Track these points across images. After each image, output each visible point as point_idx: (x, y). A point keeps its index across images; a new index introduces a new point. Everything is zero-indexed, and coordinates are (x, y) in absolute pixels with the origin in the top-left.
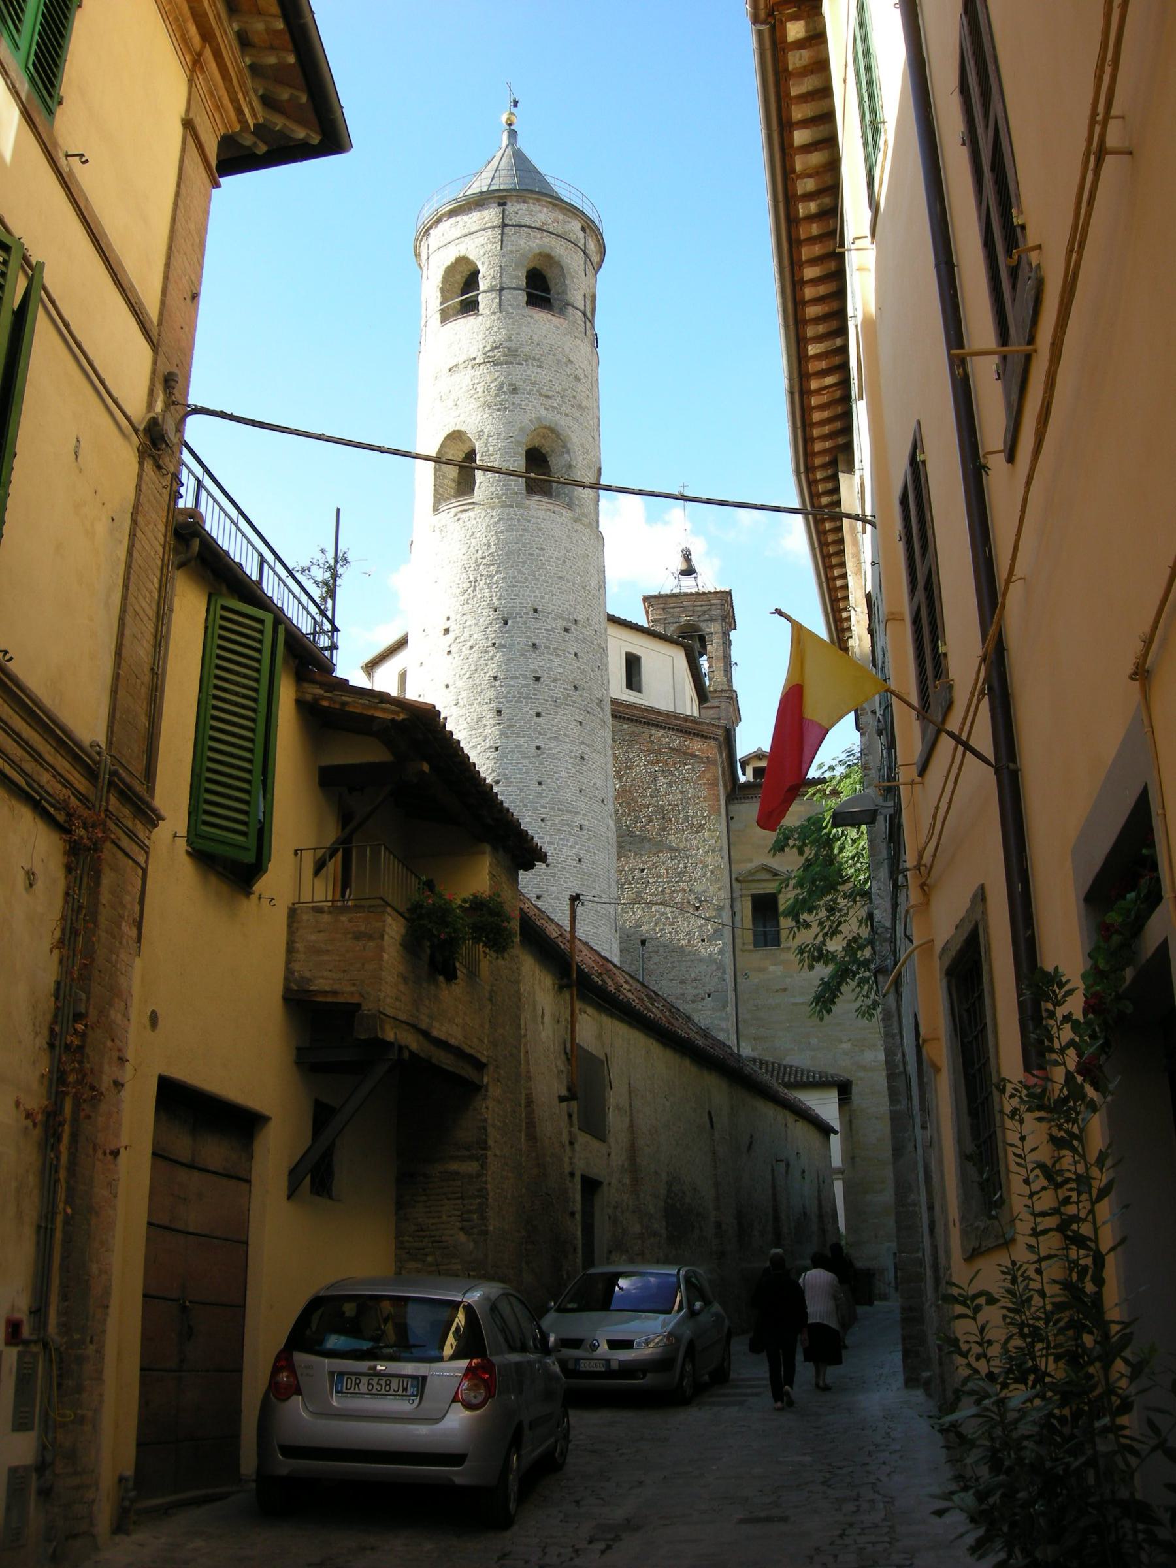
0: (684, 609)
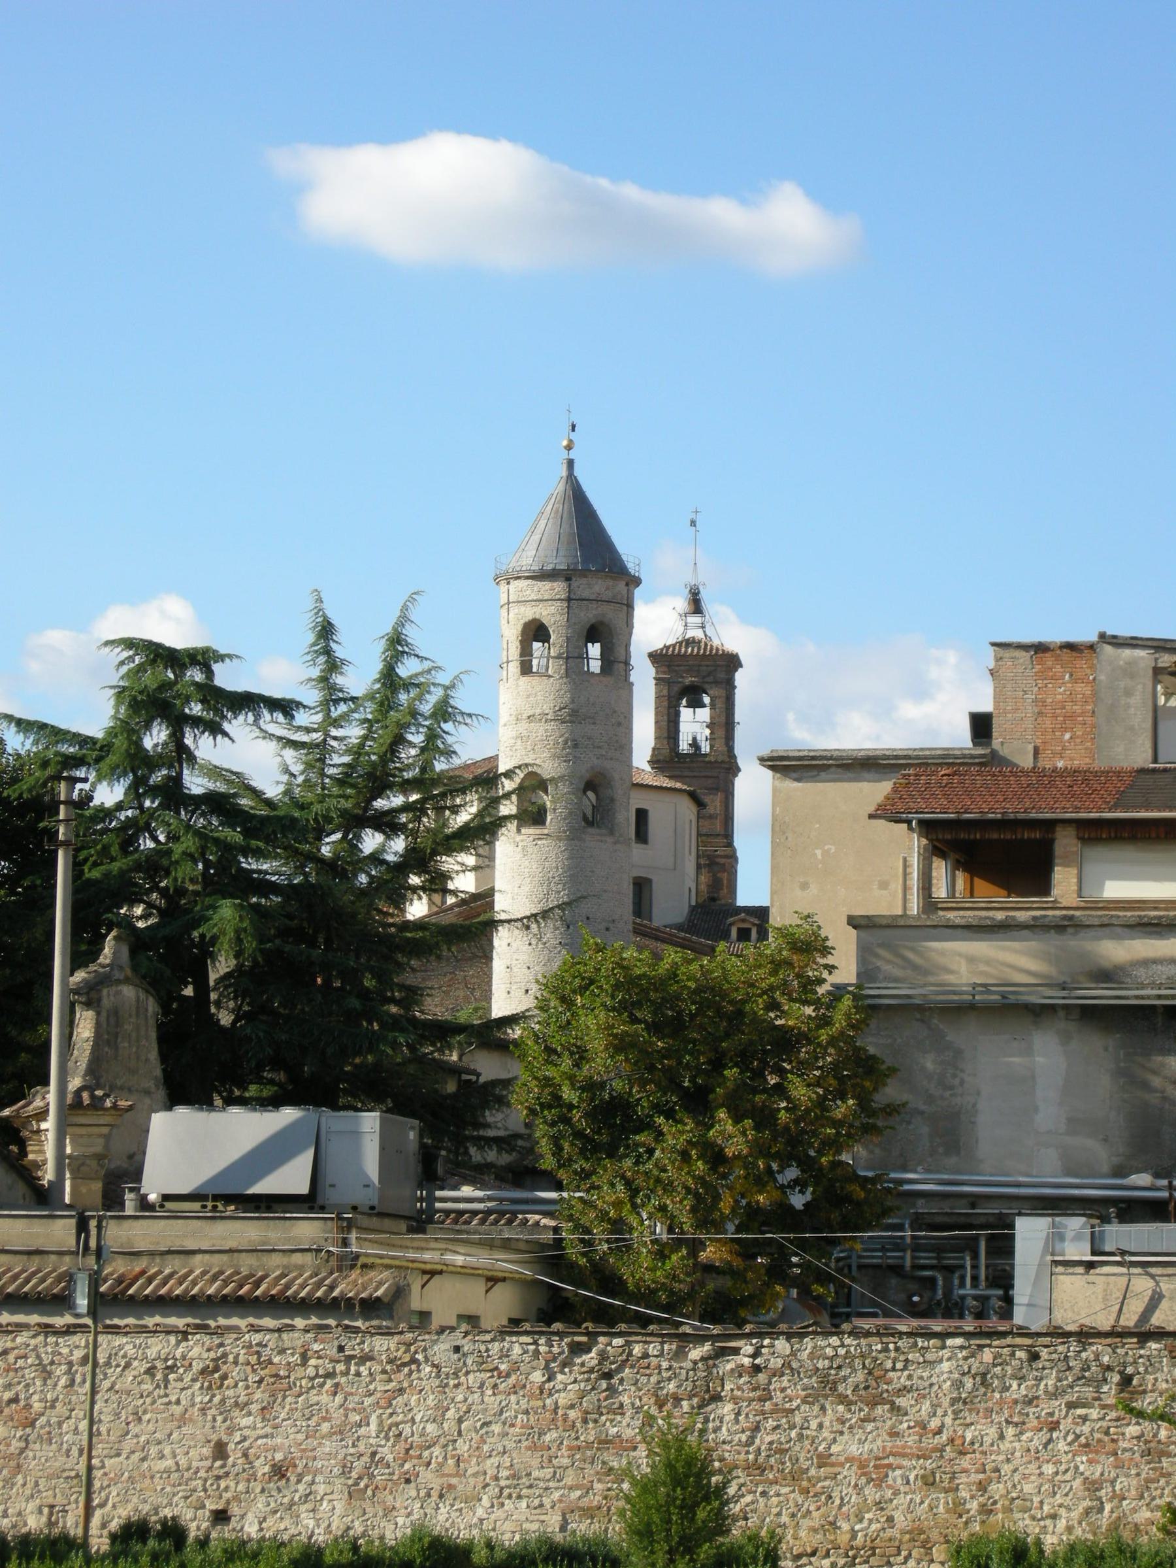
0: (690, 670)
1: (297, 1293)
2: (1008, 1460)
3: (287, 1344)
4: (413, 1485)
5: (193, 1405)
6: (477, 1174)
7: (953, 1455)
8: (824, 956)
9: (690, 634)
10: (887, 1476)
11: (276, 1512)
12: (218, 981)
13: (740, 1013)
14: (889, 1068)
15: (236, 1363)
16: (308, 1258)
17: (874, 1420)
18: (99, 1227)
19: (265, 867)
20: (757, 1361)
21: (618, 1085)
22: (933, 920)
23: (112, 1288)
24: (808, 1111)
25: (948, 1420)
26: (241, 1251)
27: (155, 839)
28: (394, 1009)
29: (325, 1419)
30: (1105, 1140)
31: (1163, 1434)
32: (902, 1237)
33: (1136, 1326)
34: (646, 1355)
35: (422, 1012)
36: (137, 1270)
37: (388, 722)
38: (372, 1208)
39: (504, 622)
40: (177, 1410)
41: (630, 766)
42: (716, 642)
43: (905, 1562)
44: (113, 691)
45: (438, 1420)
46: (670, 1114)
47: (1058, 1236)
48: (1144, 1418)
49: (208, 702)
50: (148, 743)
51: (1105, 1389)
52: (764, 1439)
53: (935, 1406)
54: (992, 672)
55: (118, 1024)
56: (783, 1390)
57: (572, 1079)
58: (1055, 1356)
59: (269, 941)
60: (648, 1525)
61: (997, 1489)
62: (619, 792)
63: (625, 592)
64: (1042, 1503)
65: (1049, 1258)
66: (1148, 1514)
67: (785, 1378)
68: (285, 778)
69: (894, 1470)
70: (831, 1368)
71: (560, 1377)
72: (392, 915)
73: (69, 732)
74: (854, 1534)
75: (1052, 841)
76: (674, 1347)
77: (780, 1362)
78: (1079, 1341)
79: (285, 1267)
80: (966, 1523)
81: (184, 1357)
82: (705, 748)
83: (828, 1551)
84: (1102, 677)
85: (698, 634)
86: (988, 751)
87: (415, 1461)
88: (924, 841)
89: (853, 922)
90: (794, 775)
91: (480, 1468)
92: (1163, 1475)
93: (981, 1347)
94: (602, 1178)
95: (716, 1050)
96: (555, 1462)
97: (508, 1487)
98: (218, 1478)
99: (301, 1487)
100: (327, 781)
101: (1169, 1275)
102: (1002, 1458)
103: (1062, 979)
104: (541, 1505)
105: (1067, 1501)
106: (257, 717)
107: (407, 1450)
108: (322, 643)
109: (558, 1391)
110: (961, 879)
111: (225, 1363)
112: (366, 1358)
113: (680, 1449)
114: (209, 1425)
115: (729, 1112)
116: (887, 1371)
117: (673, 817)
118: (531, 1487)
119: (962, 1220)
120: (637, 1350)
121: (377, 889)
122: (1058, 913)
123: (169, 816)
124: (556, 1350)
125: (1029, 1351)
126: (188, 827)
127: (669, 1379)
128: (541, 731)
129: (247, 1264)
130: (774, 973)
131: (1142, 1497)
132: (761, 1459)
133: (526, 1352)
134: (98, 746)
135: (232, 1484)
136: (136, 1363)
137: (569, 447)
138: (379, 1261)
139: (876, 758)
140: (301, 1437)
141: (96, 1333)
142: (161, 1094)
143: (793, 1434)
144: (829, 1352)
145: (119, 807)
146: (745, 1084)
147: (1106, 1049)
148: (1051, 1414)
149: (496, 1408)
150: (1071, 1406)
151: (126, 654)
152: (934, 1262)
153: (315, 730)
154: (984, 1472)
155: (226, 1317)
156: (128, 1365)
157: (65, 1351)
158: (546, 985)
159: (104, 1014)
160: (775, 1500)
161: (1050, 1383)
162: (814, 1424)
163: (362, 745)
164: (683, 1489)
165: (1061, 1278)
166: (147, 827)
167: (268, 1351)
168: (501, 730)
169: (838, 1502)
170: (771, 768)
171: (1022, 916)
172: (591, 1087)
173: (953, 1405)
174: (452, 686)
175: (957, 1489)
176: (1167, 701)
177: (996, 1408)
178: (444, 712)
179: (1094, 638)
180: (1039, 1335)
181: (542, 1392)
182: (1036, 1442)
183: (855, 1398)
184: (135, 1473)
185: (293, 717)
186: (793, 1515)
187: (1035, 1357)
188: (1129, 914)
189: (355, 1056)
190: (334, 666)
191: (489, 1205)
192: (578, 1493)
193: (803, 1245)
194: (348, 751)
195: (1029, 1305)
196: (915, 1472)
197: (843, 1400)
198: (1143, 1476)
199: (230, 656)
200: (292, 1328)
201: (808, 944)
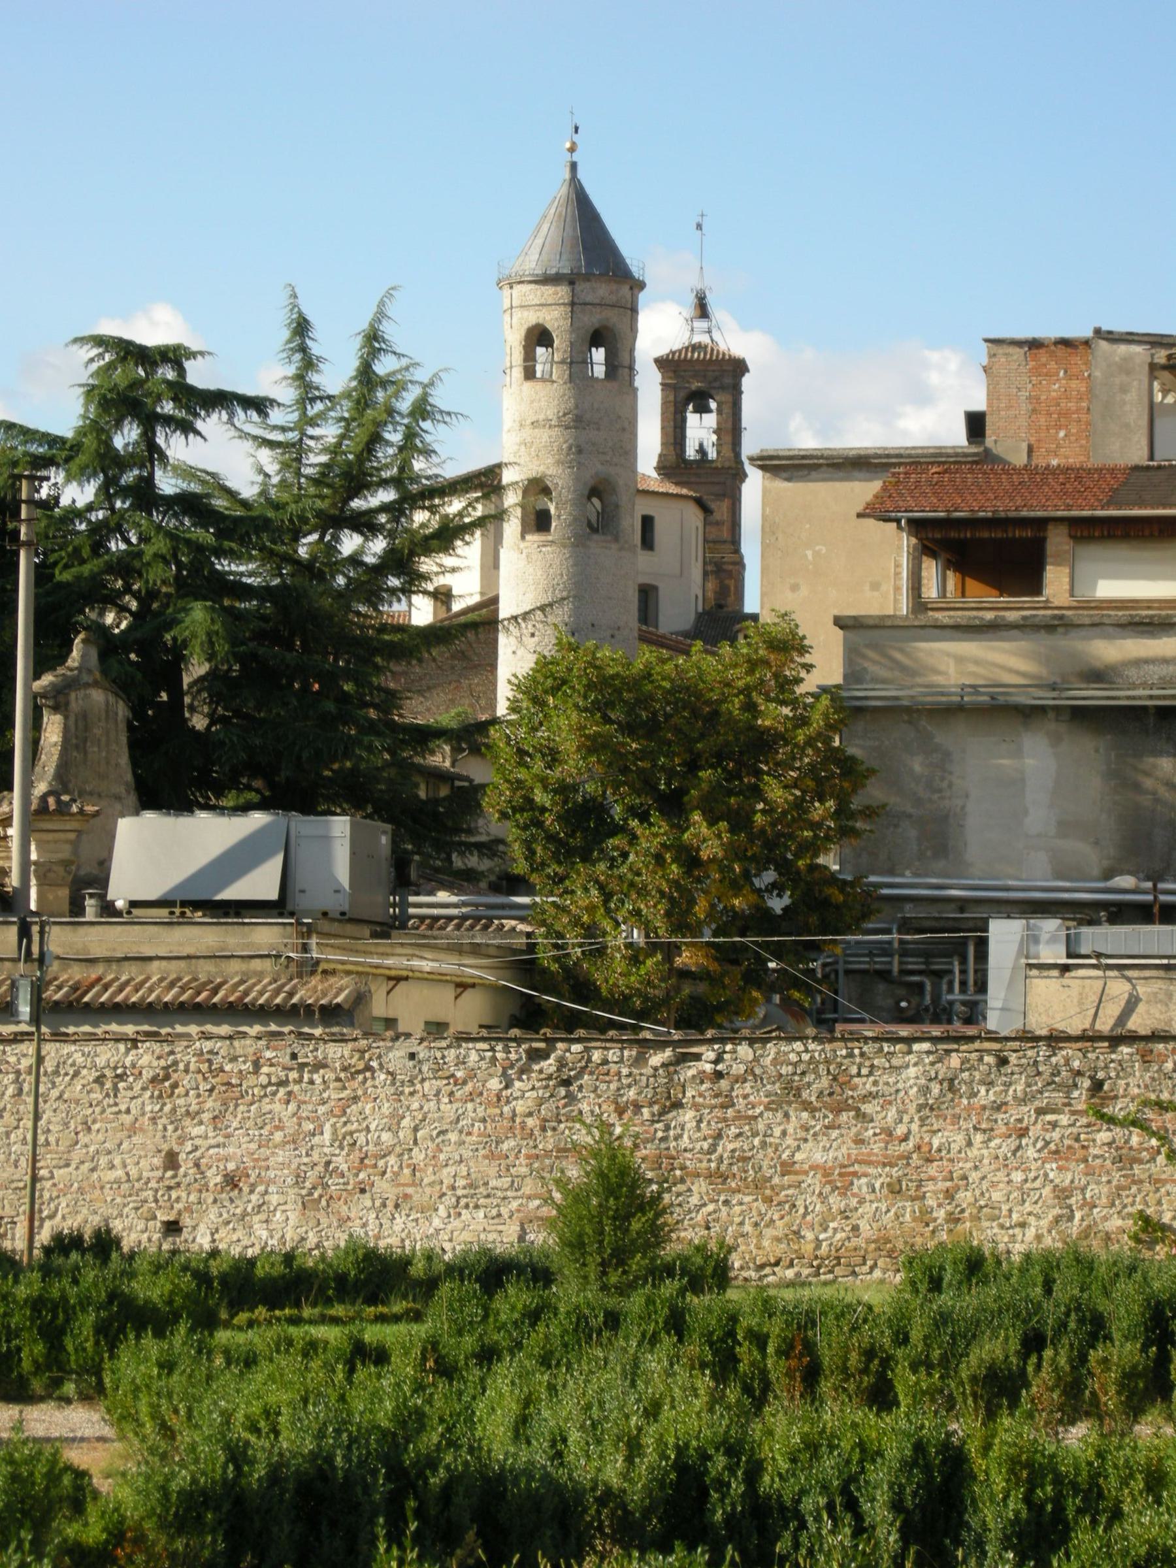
1: (255, 999)
2: (976, 1168)
3: (239, 1051)
4: (368, 1195)
5: (143, 1114)
6: (462, 880)
7: (920, 1163)
8: (802, 655)
9: (697, 339)
10: (852, 1184)
11: (228, 1223)
12: (191, 686)
13: (716, 713)
14: (867, 770)
15: (187, 1071)
16: (267, 964)
17: (839, 1127)
18: (42, 933)
19: (242, 568)
20: (720, 1067)
21: (590, 788)
22: (923, 620)
23: (67, 995)
24: (785, 813)
25: (915, 1127)
26: (198, 957)
27: (127, 541)
28: (373, 714)
29: (278, 1128)
30: (1097, 843)
31: (1135, 1140)
32: (890, 943)
33: (1112, 1030)
34: (605, 1062)
35: (400, 716)
36: (94, 976)
37: (364, 420)
38: (343, 914)
39: (507, 326)
40: (127, 1119)
41: (634, 470)
42: (722, 347)
43: (871, 1272)
44: (82, 390)
45: (394, 1129)
46: (644, 818)
47: (1032, 938)
48: (1115, 1124)
49: (180, 401)
50: (119, 442)
51: (1076, 1094)
52: (726, 1147)
53: (901, 1113)
54: (985, 369)
55: (86, 729)
56: (745, 1097)
57: (544, 782)
58: (1024, 1061)
59: (243, 643)
60: (580, 1236)
61: (964, 1197)
62: (624, 499)
63: (629, 296)
64: (1010, 1211)
65: (1023, 961)
66: (1120, 1222)
67: (748, 1085)
68: (260, 478)
69: (859, 1178)
70: (795, 1073)
71: (517, 1084)
72: (371, 617)
73: (37, 432)
74: (818, 1243)
75: (1043, 540)
76: (634, 1053)
77: (742, 1068)
78: (1049, 1046)
79: (243, 973)
80: (933, 1232)
81: (134, 1066)
82: (712, 454)
83: (792, 1261)
84: (1097, 373)
85: (704, 339)
86: (981, 449)
87: (370, 1171)
88: (914, 540)
89: (840, 622)
90: (784, 475)
91: (436, 1178)
92: (1134, 1182)
93: (948, 1052)
94: (575, 883)
95: (691, 751)
96: (513, 1170)
97: (465, 1196)
98: (170, 1188)
99: (254, 1197)
100: (303, 480)
101: (1145, 978)
102: (969, 1165)
103: (1053, 679)
104: (499, 1215)
105: (1037, 1209)
106: (232, 415)
107: (362, 1160)
108: (298, 340)
109: (516, 1099)
110: (952, 578)
111: (175, 1071)
112: (319, 1066)
113: (613, 1158)
114: (159, 1134)
115: (704, 814)
116: (852, 1077)
117: (680, 524)
118: (488, 1196)
119: (950, 924)
120: (596, 1056)
121: (354, 590)
122: (1049, 612)
123: (141, 517)
124: (513, 1056)
125: (997, 1056)
126: (159, 527)
127: (629, 1086)
128: (545, 438)
129: (205, 970)
130: (751, 672)
131: (1113, 1205)
132: (723, 1168)
133: (482, 1059)
134: (67, 446)
135: (184, 1195)
136: (84, 1072)
137: (572, 150)
138: (340, 967)
139: (867, 457)
140: (253, 1146)
141: (40, 1040)
142: (132, 799)
143: (756, 1142)
144: (793, 1057)
145: (90, 508)
146: (721, 786)
147: (1097, 751)
148: (1020, 1121)
149: (453, 1117)
150: (1040, 1112)
151: (95, 352)
152: (923, 967)
153: (291, 429)
154: (952, 1179)
155: (183, 1024)
156: (76, 1074)
157: (12, 1059)
158: (518, 686)
159: (72, 719)
160: (737, 1209)
161: (1019, 1088)
162: (777, 1132)
163: (339, 444)
164: (616, 1198)
165: (1033, 981)
166: (119, 529)
167: (220, 1059)
168: (505, 436)
169: (802, 1211)
170: (761, 467)
171: (1012, 616)
172: (564, 790)
173: (919, 1111)
174: (432, 384)
175: (924, 1197)
176: (1164, 397)
177: (964, 1114)
178: (422, 410)
179: (1088, 333)
180: (1007, 1039)
181: (499, 1100)
182: (1004, 1149)
183: (818, 1105)
184: (85, 1184)
185: (267, 415)
186: (756, 1225)
187: (1003, 1062)
188: (1120, 613)
189: (333, 762)
190: (309, 363)
191: (464, 910)
192: (537, 1202)
193: (778, 952)
194: (325, 450)
195: (1002, 1009)
196: (881, 1180)
197: (807, 1106)
198: (1115, 1183)
199: (202, 353)
200: (244, 1035)
201: (785, 642)
